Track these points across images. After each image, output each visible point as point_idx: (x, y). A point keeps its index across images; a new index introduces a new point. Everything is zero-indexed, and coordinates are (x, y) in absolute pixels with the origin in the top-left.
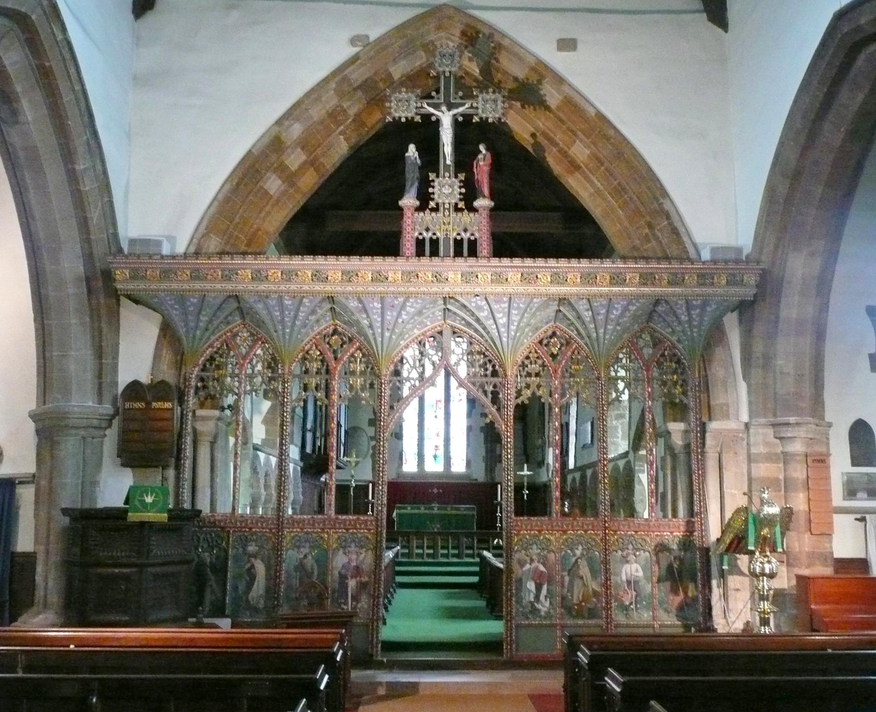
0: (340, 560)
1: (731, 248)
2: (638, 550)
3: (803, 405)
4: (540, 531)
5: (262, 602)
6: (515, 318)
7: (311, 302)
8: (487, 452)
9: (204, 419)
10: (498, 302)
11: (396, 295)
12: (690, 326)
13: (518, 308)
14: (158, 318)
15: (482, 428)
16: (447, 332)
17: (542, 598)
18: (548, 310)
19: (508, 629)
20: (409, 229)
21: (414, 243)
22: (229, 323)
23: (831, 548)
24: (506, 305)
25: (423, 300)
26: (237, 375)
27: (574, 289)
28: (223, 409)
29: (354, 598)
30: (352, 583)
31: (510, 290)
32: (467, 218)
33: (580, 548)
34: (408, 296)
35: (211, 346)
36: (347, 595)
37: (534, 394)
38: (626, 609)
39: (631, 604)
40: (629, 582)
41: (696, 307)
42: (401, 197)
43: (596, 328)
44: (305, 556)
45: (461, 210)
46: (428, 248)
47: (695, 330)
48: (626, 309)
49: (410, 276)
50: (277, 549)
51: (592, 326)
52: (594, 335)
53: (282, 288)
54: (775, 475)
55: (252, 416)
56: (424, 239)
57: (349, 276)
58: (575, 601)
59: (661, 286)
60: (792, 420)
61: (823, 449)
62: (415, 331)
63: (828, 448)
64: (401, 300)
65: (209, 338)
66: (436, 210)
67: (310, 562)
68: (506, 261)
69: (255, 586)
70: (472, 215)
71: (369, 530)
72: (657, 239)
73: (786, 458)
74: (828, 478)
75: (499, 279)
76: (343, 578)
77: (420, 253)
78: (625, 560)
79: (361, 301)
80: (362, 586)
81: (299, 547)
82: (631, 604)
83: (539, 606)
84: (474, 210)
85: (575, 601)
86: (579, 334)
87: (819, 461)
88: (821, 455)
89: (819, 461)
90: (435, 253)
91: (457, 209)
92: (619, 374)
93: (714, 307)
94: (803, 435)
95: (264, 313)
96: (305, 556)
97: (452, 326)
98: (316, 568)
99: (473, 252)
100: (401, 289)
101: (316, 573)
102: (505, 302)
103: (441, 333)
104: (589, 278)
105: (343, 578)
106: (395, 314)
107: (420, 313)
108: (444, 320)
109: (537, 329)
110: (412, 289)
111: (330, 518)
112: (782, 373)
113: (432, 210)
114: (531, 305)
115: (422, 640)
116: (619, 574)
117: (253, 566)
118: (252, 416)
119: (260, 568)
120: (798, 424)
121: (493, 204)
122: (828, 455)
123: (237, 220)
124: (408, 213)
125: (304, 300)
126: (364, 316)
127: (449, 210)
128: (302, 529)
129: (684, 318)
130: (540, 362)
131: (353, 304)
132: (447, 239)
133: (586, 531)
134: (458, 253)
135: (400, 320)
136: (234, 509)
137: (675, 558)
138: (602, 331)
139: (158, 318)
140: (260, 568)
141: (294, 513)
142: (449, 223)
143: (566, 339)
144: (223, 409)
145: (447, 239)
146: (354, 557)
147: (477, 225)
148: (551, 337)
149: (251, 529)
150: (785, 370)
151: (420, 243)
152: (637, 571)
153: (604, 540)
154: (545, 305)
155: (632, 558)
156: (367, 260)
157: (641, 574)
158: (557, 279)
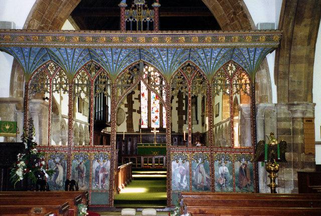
0: (96, 165)
1: (270, 23)
2: (227, 160)
3: (301, 95)
4: (183, 152)
5: (62, 183)
6: (170, 58)
7: (79, 51)
8: (179, 119)
9: (35, 103)
10: (162, 51)
11: (117, 48)
12: (250, 60)
13: (171, 53)
14: (12, 58)
15: (176, 108)
16: (142, 65)
17: (184, 181)
18: (185, 54)
19: (169, 195)
20: (123, 17)
21: (125, 24)
22: (44, 60)
23: (315, 160)
24: (166, 52)
25: (129, 50)
26: (49, 84)
27: (195, 45)
28: (44, 99)
29: (102, 181)
30: (101, 175)
31: (166, 45)
32: (148, 12)
33: (200, 159)
34: (122, 48)
35: (37, 70)
36: (99, 180)
37: (180, 91)
38: (221, 186)
39: (223, 184)
40: (222, 174)
41: (251, 52)
42: (119, 3)
43: (207, 62)
44: (81, 163)
45: (146, 9)
46: (132, 26)
47: (252, 62)
48: (219, 53)
49: (122, 40)
50: (69, 160)
51: (205, 61)
52: (206, 65)
53: (66, 45)
54: (288, 127)
55: (61, 103)
56: (136, 21)
57: (95, 39)
58: (198, 182)
59: (235, 42)
60: (295, 103)
61: (311, 116)
62: (127, 64)
63: (314, 115)
64: (119, 50)
65: (35, 67)
66: (135, 8)
67: (82, 166)
68: (165, 32)
69: (58, 177)
70: (151, 10)
71: (108, 152)
72: (237, 19)
73: (294, 120)
74: (313, 129)
75: (162, 40)
76: (97, 172)
77: (128, 28)
78: (220, 165)
79: (102, 51)
80: (106, 176)
81: (78, 159)
82: (223, 184)
83: (182, 185)
84: (152, 8)
85: (198, 182)
86: (200, 65)
87: (309, 121)
88: (311, 118)
89: (309, 121)
90: (134, 29)
91: (144, 8)
92: (218, 82)
93: (260, 51)
94: (301, 109)
95: (59, 56)
96: (81, 163)
97: (143, 61)
98: (85, 168)
99: (151, 29)
100: (119, 45)
101: (85, 170)
102: (165, 51)
103: (139, 65)
104: (202, 39)
105: (97, 172)
106: (117, 56)
107: (128, 56)
108: (140, 59)
109: (180, 63)
110: (124, 45)
111: (91, 146)
112: (292, 81)
113: (133, 8)
114: (177, 52)
115: (130, 199)
116: (218, 171)
117: (57, 168)
118: (61, 103)
119: (61, 169)
120: (298, 104)
121: (67, 20)
122: (314, 118)
123: (46, 13)
124: (122, 10)
125: (76, 50)
126: (104, 57)
127: (141, 8)
128: (79, 151)
129: (247, 56)
130: (182, 77)
131: (98, 52)
132: (140, 22)
133: (203, 152)
134: (145, 29)
135: (120, 59)
136: (49, 144)
137: (243, 164)
138: (209, 63)
139: (12, 58)
140: (61, 169)
141: (86, 144)
142: (141, 15)
143: (194, 67)
144: (44, 99)
145: (140, 22)
146: (102, 163)
147: (149, 16)
148: (187, 66)
149: (56, 152)
150: (293, 80)
151: (128, 24)
152: (226, 170)
153: (211, 156)
154: (183, 52)
155: (223, 164)
156: (103, 32)
157: (228, 171)
158: (175, 40)
